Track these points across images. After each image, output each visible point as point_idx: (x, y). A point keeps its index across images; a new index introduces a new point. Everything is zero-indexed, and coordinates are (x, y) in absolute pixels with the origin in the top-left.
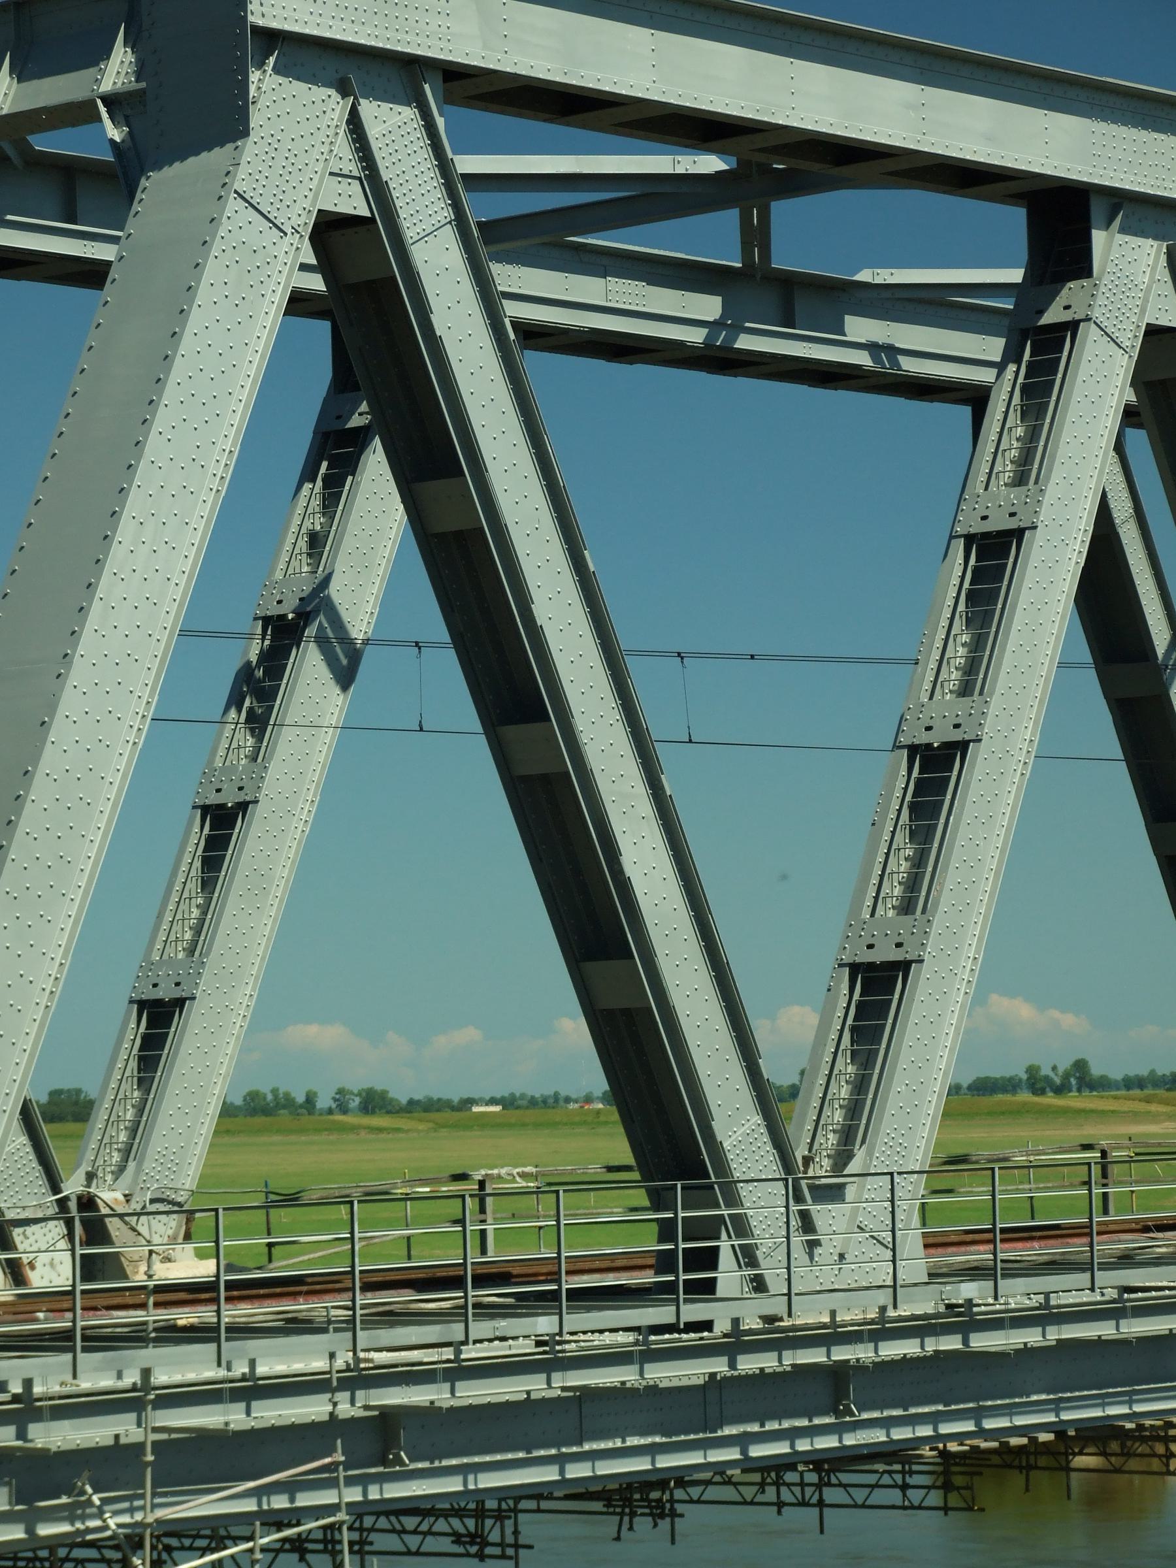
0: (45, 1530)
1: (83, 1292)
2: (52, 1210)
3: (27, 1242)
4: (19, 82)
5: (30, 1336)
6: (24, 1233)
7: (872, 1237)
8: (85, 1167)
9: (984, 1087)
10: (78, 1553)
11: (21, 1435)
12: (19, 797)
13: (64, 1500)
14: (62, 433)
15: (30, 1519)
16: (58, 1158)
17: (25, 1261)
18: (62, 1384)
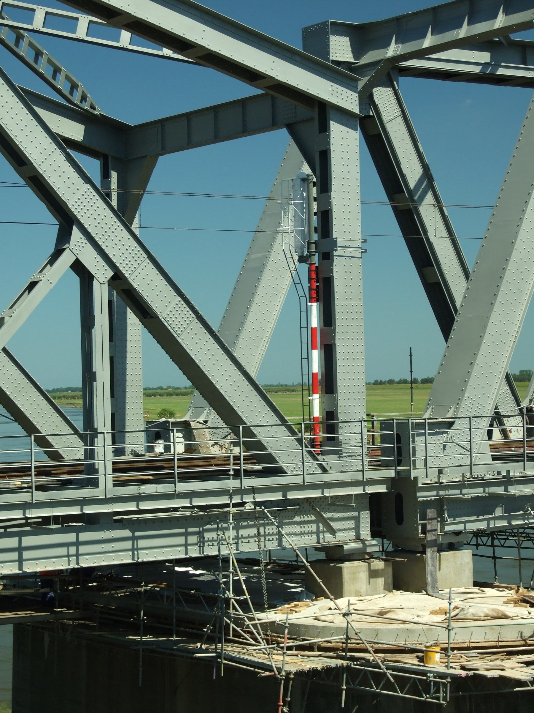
0: (514, 523)
1: (527, 441)
2: (517, 413)
3: (508, 423)
4: (506, 16)
5: (509, 456)
6: (508, 420)
7: (457, 444)
8: (529, 397)
9: (376, 383)
10: (527, 531)
11: (506, 490)
12: (504, 268)
13: (521, 512)
14: (520, 140)
15: (509, 519)
16: (519, 394)
17: (508, 430)
18: (520, 472)
